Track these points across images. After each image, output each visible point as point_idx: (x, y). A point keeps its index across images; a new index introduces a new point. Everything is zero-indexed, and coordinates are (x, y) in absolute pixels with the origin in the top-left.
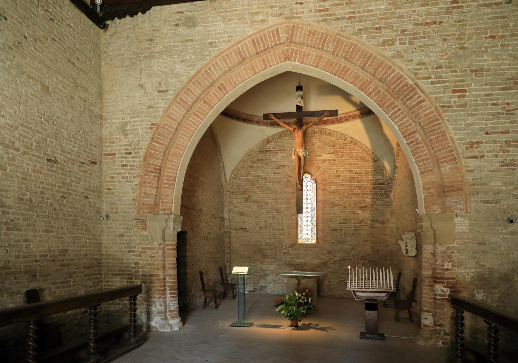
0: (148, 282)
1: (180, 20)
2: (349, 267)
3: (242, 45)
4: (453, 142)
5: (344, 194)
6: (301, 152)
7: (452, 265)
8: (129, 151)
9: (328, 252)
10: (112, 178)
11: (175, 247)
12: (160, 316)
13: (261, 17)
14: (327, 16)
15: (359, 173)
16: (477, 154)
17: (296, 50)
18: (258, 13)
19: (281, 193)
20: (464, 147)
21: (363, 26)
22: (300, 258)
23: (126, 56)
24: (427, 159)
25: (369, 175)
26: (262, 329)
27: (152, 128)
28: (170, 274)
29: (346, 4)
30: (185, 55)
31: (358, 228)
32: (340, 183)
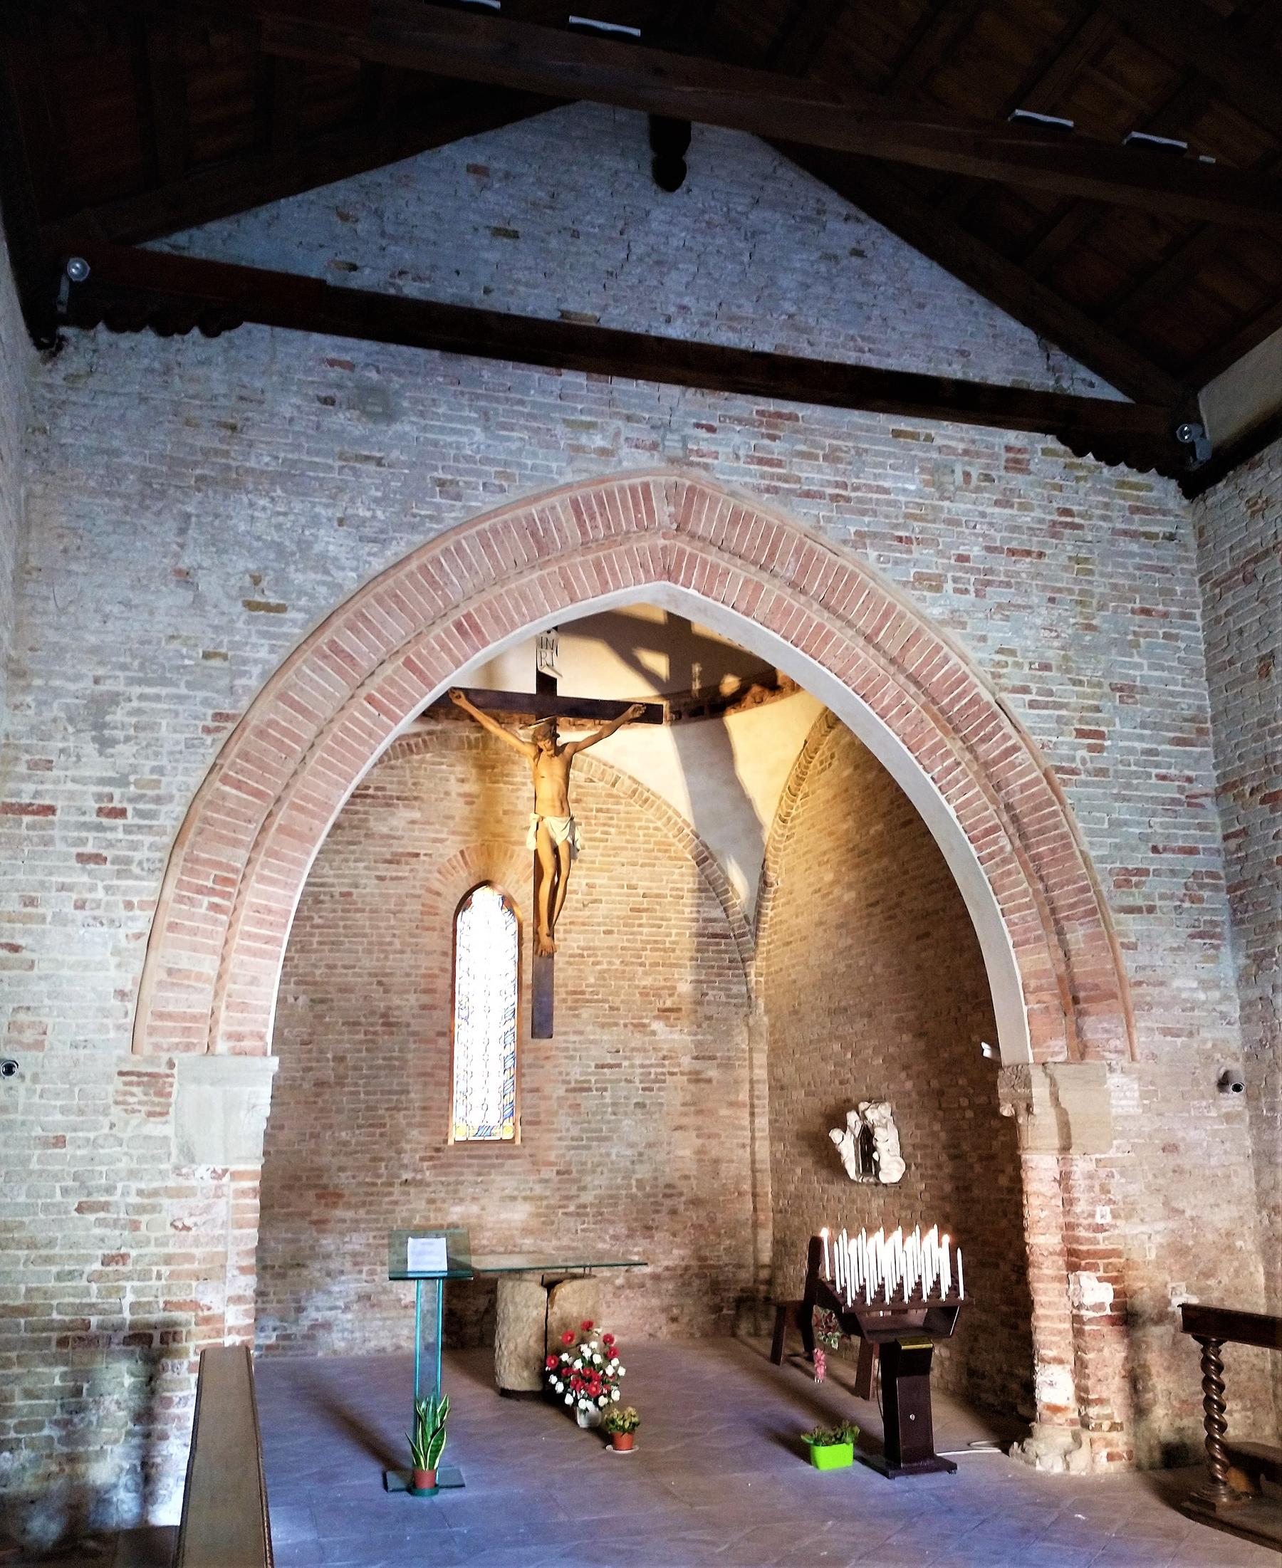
1: (340, 387)
3: (543, 511)
5: (610, 963)
8: (116, 804)
9: (558, 1173)
10: (31, 902)
13: (598, 441)
15: (658, 896)
16: (1140, 902)
19: (402, 952)
23: (127, 459)
27: (217, 729)
29: (825, 458)
30: (352, 500)
31: (655, 1081)
32: (599, 924)
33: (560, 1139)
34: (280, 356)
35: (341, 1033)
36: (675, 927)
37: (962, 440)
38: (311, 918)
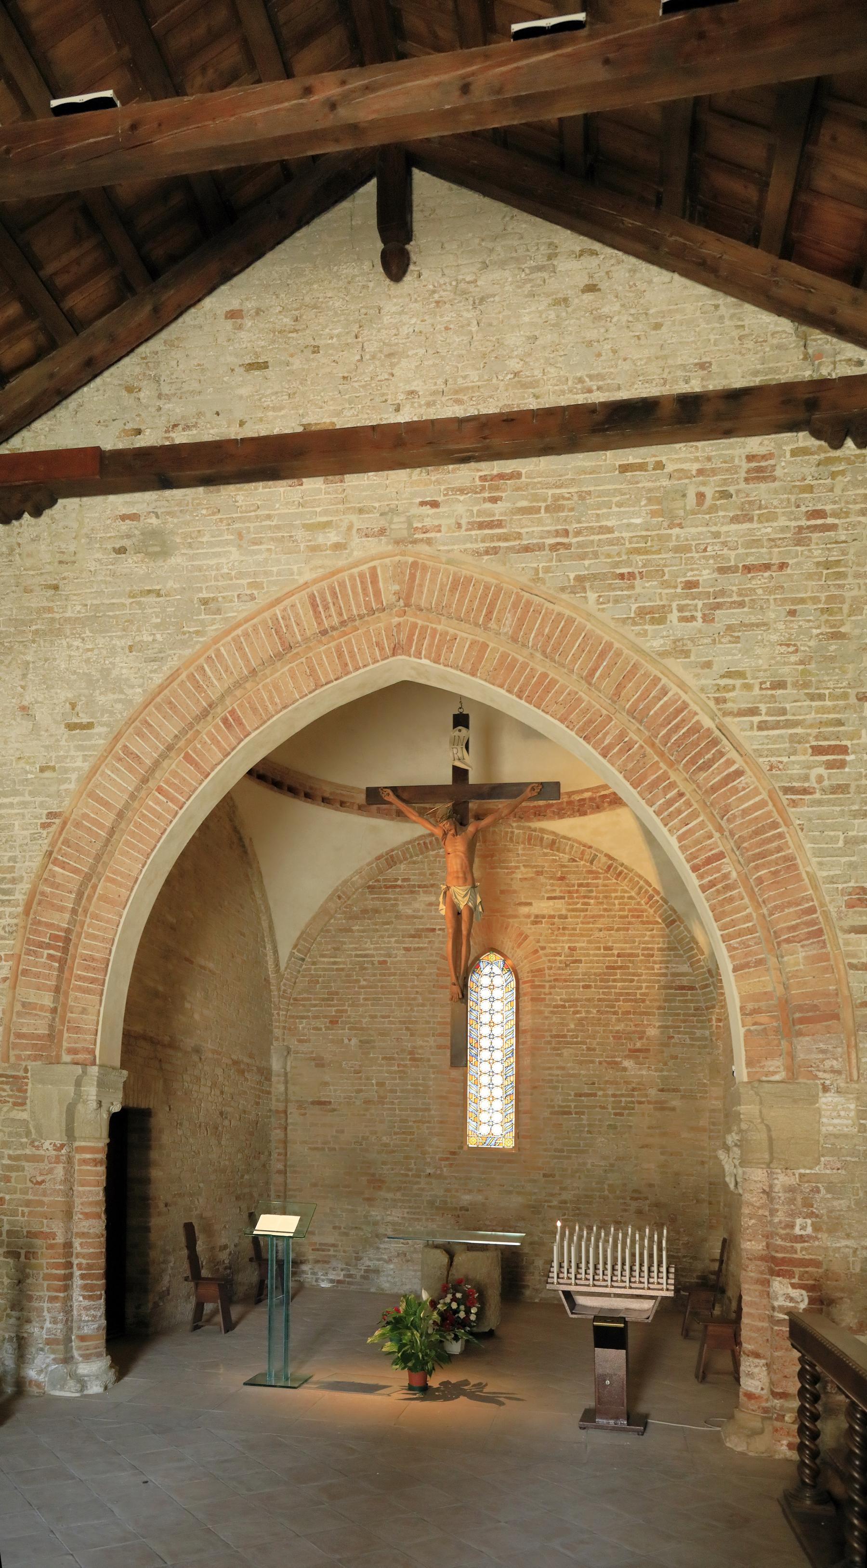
0: (23, 1252)
1: (128, 536)
2: (559, 1224)
3: (285, 610)
4: (815, 887)
5: (588, 1012)
6: (461, 896)
7: (813, 1224)
11: (102, 1156)
12: (53, 1352)
13: (333, 537)
14: (499, 540)
17: (422, 627)
18: (327, 525)
19: (423, 1005)
20: (842, 901)
21: (587, 569)
22: (470, 1191)
24: (751, 931)
25: (655, 962)
26: (327, 1394)
28: (89, 1230)
31: (624, 1108)
32: (579, 980)
33: (545, 1150)
34: (87, 520)
35: (382, 1066)
36: (645, 981)
37: (697, 459)
38: (358, 981)
